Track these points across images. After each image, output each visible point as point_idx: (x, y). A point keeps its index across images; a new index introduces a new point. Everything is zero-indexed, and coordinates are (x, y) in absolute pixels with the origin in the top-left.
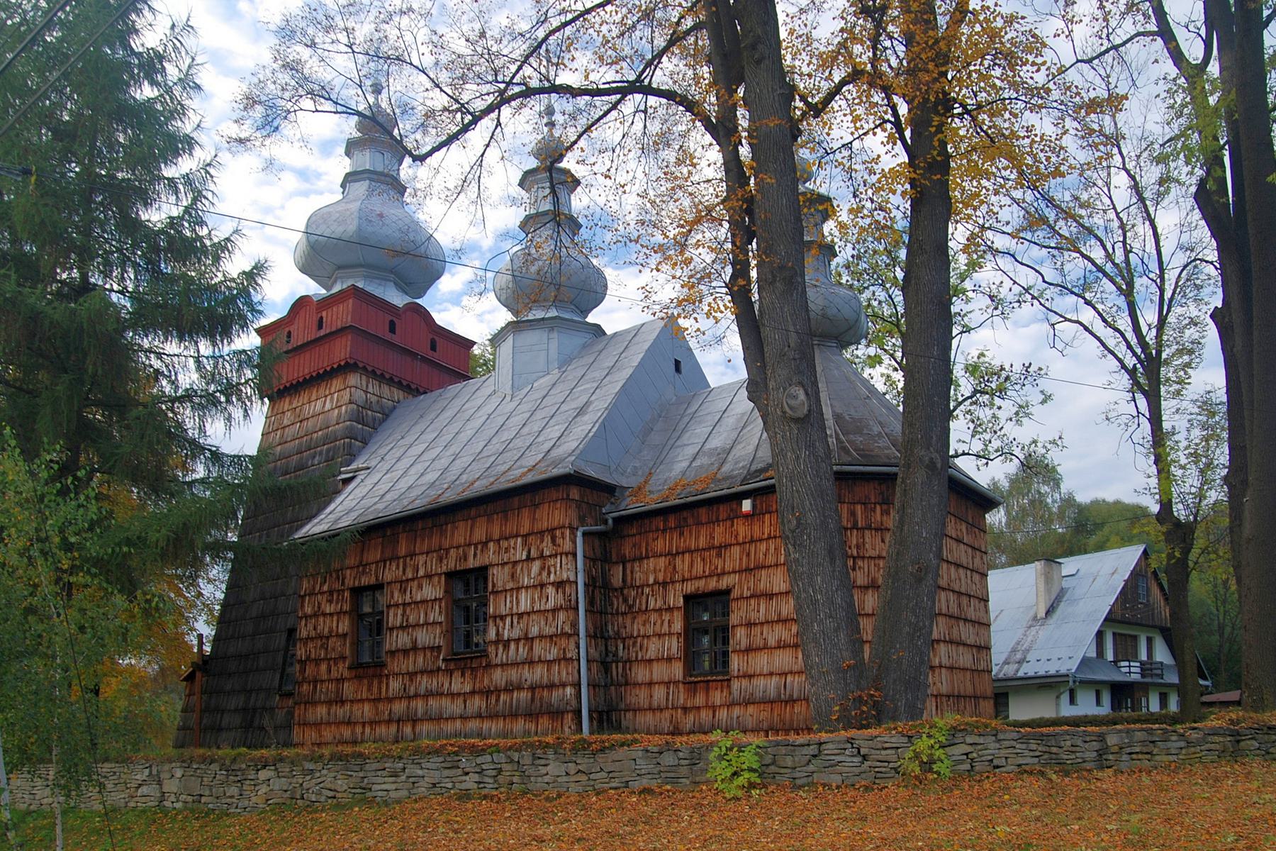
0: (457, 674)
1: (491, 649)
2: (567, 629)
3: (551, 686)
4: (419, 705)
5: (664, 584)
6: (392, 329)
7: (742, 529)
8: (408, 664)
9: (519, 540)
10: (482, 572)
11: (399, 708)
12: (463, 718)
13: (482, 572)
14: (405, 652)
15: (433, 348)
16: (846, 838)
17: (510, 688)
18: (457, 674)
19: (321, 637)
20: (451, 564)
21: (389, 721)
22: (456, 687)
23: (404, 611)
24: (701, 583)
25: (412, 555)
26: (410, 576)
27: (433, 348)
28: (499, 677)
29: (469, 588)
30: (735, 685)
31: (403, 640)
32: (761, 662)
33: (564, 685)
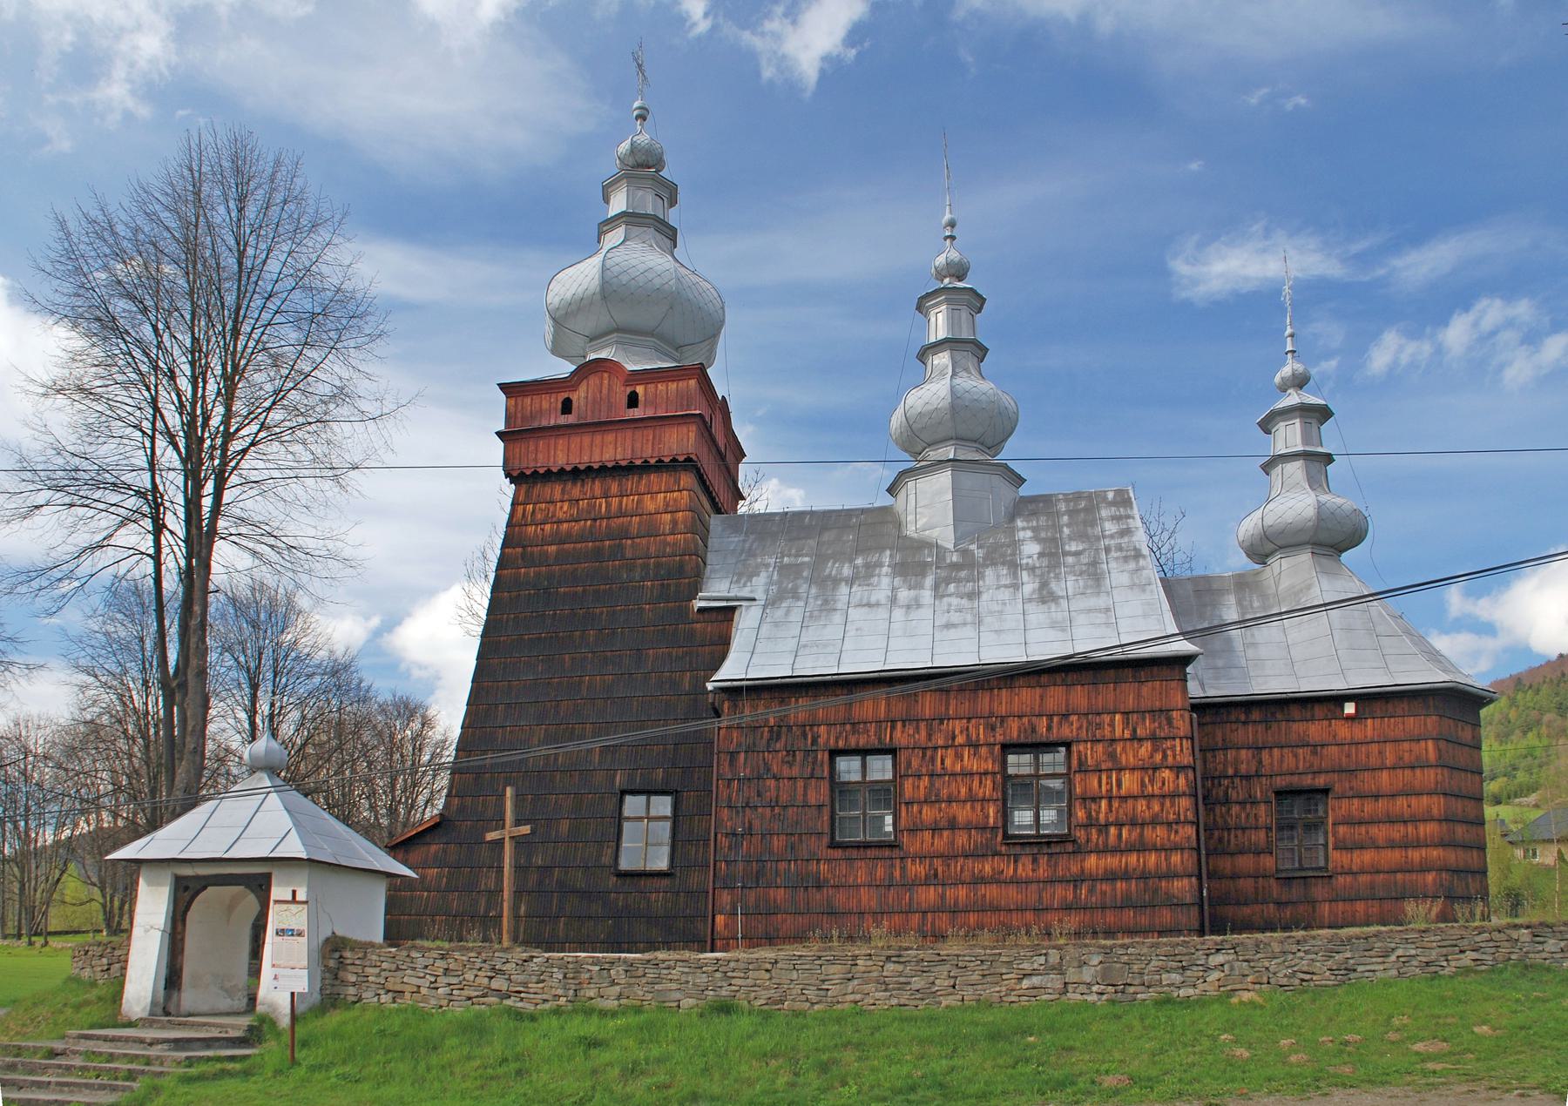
5: (1247, 777)
9: (1118, 717)
17: (1111, 877)
23: (932, 784)
26: (940, 742)
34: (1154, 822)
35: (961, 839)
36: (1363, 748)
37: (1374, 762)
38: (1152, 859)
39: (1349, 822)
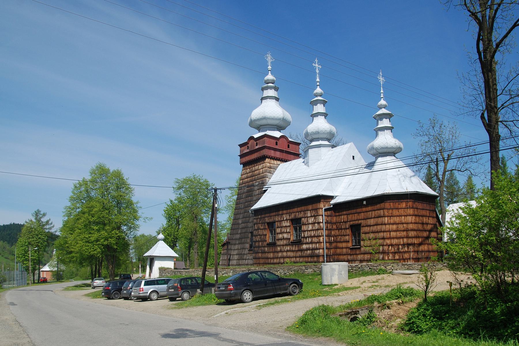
0: (294, 246)
1: (302, 239)
2: (514, 134)
3: (317, 249)
4: (285, 254)
5: (345, 222)
6: (277, 144)
7: (364, 209)
8: (281, 243)
10: (300, 219)
11: (280, 255)
12: (296, 257)
13: (300, 219)
14: (281, 239)
15: (288, 147)
16: (123, 188)
18: (294, 246)
19: (260, 235)
20: (293, 216)
21: (277, 258)
22: (294, 249)
24: (354, 222)
25: (283, 214)
27: (288, 147)
28: (304, 246)
29: (296, 223)
30: (362, 249)
31: (280, 236)
32: (367, 243)
33: (320, 249)
34: (314, 236)
35: (285, 242)
36: (368, 213)
37: (370, 216)
38: (314, 245)
39: (366, 233)
